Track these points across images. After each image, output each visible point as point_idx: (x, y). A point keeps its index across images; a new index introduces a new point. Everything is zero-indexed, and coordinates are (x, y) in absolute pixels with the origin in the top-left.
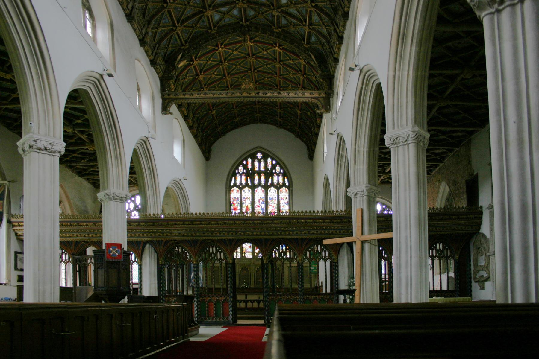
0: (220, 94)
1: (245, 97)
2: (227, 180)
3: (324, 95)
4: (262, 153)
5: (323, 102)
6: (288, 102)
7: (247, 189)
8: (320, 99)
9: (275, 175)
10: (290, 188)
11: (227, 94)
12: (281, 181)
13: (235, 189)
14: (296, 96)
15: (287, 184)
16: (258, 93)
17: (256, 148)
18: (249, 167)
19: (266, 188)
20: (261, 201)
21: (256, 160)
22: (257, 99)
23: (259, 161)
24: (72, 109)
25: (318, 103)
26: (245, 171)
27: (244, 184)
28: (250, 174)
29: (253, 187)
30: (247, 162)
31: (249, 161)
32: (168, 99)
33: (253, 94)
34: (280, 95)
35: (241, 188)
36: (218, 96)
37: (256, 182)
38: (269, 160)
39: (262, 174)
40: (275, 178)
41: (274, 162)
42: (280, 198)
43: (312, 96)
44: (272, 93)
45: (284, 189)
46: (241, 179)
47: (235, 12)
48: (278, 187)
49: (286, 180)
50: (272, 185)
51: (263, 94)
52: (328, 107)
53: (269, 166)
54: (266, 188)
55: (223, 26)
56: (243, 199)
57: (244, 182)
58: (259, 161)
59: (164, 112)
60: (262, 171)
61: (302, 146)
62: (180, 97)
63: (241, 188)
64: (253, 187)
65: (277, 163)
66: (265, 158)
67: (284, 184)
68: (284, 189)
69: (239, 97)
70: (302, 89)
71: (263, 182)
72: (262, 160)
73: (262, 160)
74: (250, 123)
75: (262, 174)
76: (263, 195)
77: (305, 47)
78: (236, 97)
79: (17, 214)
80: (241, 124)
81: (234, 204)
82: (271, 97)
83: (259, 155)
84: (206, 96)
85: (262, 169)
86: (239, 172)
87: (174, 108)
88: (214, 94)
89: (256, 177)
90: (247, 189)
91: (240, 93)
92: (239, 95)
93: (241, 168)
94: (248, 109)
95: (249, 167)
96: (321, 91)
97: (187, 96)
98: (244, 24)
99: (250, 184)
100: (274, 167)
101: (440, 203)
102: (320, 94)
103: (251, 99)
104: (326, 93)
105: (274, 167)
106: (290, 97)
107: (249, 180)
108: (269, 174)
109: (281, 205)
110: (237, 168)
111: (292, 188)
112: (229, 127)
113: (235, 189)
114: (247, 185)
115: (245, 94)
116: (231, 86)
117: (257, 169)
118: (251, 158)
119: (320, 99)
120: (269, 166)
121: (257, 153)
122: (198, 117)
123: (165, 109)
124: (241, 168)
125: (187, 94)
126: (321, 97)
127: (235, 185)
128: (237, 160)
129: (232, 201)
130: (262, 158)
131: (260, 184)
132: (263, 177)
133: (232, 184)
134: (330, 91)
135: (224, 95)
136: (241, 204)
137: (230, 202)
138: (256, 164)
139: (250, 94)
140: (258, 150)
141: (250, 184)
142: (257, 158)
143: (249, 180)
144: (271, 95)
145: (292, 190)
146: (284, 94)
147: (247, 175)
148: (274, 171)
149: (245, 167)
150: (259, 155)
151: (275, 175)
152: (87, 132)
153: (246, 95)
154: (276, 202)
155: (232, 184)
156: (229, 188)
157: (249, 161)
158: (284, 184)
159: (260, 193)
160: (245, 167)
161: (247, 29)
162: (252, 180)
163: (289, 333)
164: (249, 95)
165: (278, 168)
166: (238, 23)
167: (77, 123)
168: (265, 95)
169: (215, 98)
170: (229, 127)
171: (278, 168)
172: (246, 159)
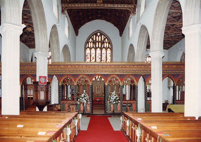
0: (87, 5)
1: (98, 7)
2: (85, 45)
3: (133, 7)
4: (100, 33)
6: (112, 9)
7: (93, 49)
8: (132, 9)
9: (105, 43)
10: (111, 49)
11: (91, 5)
12: (108, 46)
13: (88, 49)
14: (121, 7)
15: (110, 47)
16: (104, 5)
17: (98, 30)
18: (94, 39)
19: (101, 49)
20: (99, 55)
21: (97, 36)
22: (104, 8)
23: (99, 37)
25: (131, 10)
26: (92, 41)
27: (92, 47)
28: (94, 42)
29: (96, 48)
30: (93, 37)
31: (94, 36)
32: (64, 7)
33: (102, 6)
34: (114, 6)
35: (91, 49)
36: (86, 6)
37: (97, 46)
38: (103, 36)
39: (100, 43)
40: (105, 44)
41: (105, 37)
42: (107, 54)
43: (128, 7)
44: (111, 5)
45: (109, 49)
46: (91, 45)
48: (106, 49)
49: (110, 45)
50: (104, 47)
51: (106, 5)
52: (135, 12)
53: (103, 39)
54: (101, 49)
56: (91, 54)
57: (92, 46)
58: (99, 37)
59: (62, 13)
60: (100, 41)
61: (117, 31)
62: (69, 6)
63: (91, 49)
64: (96, 48)
65: (107, 38)
66: (101, 35)
67: (109, 47)
68: (109, 49)
69: (96, 7)
70: (120, 4)
71: (100, 46)
72: (100, 36)
73: (100, 36)
74: (95, 19)
75: (100, 43)
76: (100, 52)
78: (94, 7)
80: (100, 18)
81: (88, 56)
82: (84, 7)
83: (99, 34)
84: (93, 6)
85: (100, 40)
86: (90, 42)
87: (66, 12)
89: (97, 44)
90: (93, 49)
91: (96, 5)
92: (96, 6)
93: (91, 39)
94: (95, 13)
95: (94, 39)
96: (132, 5)
97: (73, 6)
99: (94, 47)
100: (105, 39)
103: (101, 8)
104: (134, 6)
105: (105, 39)
106: (118, 7)
107: (94, 45)
108: (103, 43)
109: (107, 56)
110: (89, 39)
111: (112, 49)
112: (86, 21)
113: (88, 49)
114: (93, 47)
115: (98, 5)
116: (90, 2)
117: (97, 40)
118: (95, 35)
119: (132, 9)
120: (103, 39)
121: (98, 33)
122: (75, 16)
123: (63, 11)
124: (91, 39)
125: (73, 5)
127: (88, 47)
128: (89, 36)
129: (87, 54)
130: (100, 35)
131: (98, 47)
132: (100, 44)
133: (87, 47)
135: (89, 6)
136: (91, 56)
137: (86, 55)
138: (97, 38)
139: (101, 5)
140: (98, 32)
141: (94, 47)
142: (98, 35)
143: (94, 45)
144: (110, 6)
145: (112, 50)
146: (116, 6)
147: (93, 43)
148: (105, 41)
149: (93, 39)
150: (99, 34)
151: (105, 43)
152: (28, 22)
153: (99, 6)
154: (105, 55)
155: (87, 47)
156: (86, 49)
157: (94, 36)
158: (109, 47)
159: (98, 51)
160: (93, 39)
162: (96, 45)
163: (132, 86)
164: (100, 6)
165: (106, 40)
167: (24, 18)
169: (85, 7)
170: (86, 21)
171: (106, 40)
172: (93, 36)
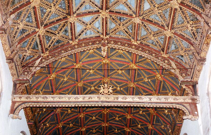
3: (190, 101)
5: (189, 107)
14: (159, 101)
16: (117, 98)
24: (80, 94)
25: (184, 109)
36: (74, 100)
44: (133, 98)
47: (98, 24)
52: (196, 113)
55: (84, 39)
69: (97, 102)
77: (163, 57)
79: (167, 31)
88: (69, 98)
98: (104, 37)
101: (15, 79)
102: (184, 99)
126: (186, 103)
134: (195, 97)
161: (106, 41)
166: (100, 36)
168: (124, 100)
